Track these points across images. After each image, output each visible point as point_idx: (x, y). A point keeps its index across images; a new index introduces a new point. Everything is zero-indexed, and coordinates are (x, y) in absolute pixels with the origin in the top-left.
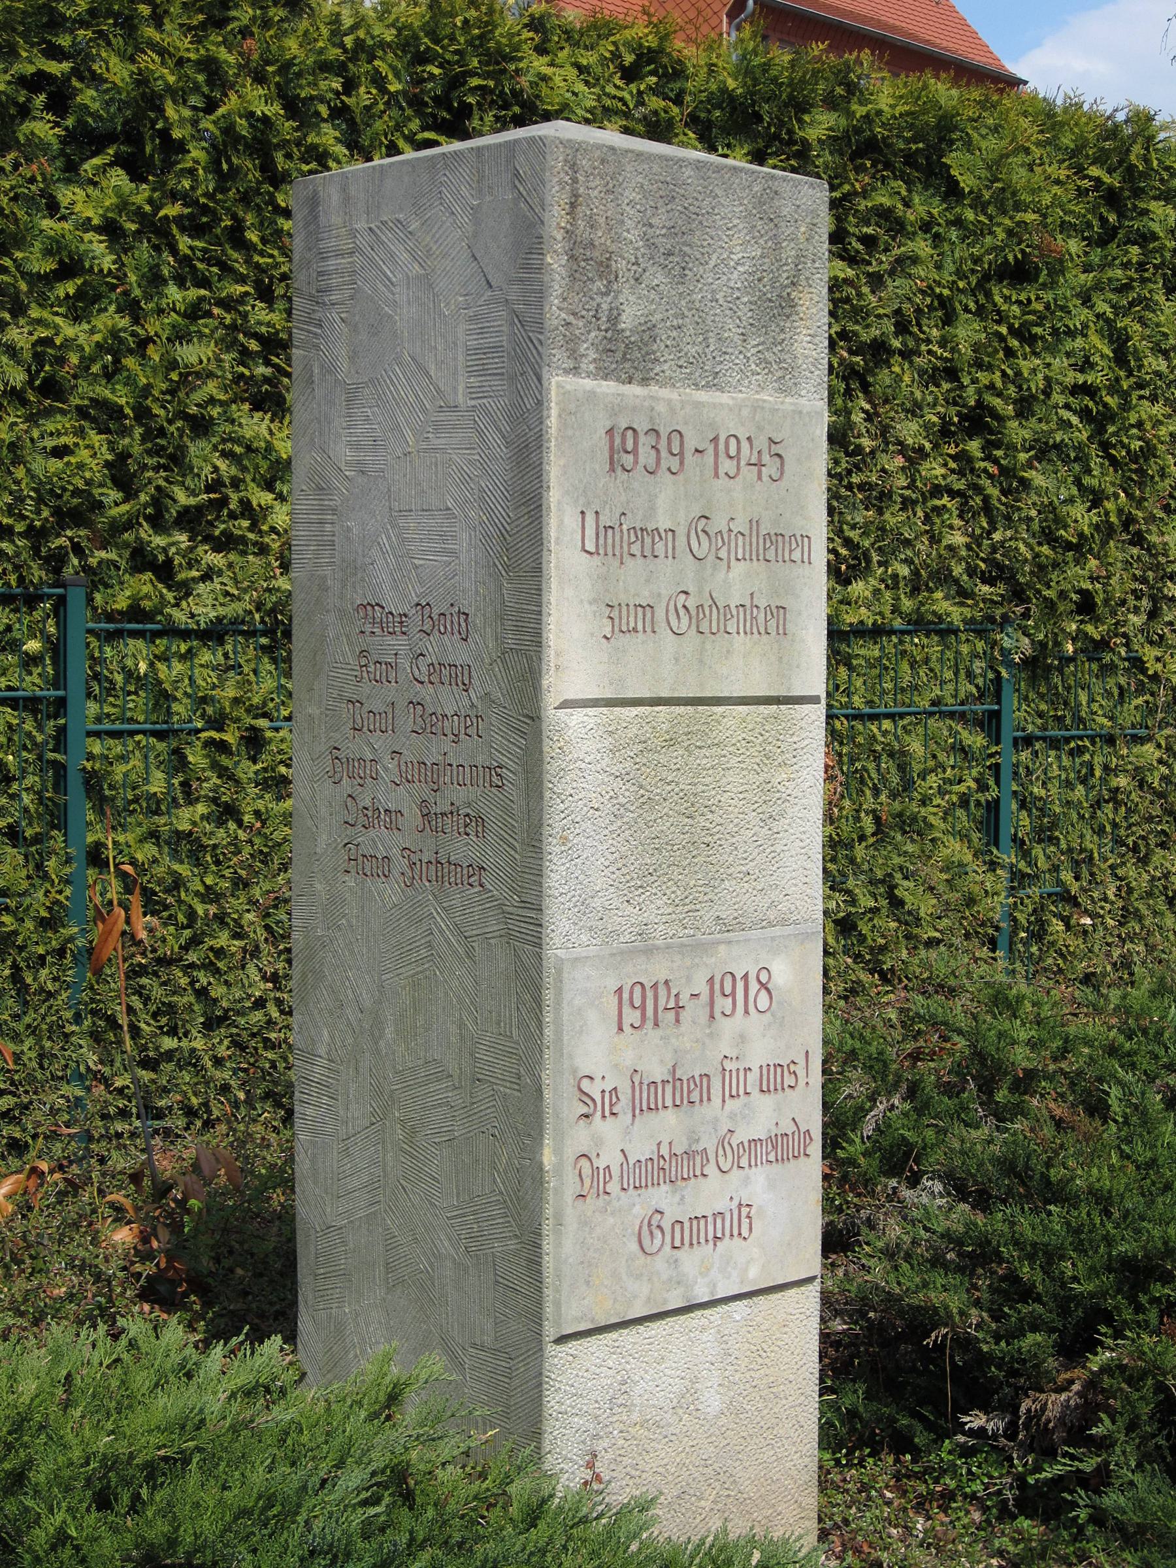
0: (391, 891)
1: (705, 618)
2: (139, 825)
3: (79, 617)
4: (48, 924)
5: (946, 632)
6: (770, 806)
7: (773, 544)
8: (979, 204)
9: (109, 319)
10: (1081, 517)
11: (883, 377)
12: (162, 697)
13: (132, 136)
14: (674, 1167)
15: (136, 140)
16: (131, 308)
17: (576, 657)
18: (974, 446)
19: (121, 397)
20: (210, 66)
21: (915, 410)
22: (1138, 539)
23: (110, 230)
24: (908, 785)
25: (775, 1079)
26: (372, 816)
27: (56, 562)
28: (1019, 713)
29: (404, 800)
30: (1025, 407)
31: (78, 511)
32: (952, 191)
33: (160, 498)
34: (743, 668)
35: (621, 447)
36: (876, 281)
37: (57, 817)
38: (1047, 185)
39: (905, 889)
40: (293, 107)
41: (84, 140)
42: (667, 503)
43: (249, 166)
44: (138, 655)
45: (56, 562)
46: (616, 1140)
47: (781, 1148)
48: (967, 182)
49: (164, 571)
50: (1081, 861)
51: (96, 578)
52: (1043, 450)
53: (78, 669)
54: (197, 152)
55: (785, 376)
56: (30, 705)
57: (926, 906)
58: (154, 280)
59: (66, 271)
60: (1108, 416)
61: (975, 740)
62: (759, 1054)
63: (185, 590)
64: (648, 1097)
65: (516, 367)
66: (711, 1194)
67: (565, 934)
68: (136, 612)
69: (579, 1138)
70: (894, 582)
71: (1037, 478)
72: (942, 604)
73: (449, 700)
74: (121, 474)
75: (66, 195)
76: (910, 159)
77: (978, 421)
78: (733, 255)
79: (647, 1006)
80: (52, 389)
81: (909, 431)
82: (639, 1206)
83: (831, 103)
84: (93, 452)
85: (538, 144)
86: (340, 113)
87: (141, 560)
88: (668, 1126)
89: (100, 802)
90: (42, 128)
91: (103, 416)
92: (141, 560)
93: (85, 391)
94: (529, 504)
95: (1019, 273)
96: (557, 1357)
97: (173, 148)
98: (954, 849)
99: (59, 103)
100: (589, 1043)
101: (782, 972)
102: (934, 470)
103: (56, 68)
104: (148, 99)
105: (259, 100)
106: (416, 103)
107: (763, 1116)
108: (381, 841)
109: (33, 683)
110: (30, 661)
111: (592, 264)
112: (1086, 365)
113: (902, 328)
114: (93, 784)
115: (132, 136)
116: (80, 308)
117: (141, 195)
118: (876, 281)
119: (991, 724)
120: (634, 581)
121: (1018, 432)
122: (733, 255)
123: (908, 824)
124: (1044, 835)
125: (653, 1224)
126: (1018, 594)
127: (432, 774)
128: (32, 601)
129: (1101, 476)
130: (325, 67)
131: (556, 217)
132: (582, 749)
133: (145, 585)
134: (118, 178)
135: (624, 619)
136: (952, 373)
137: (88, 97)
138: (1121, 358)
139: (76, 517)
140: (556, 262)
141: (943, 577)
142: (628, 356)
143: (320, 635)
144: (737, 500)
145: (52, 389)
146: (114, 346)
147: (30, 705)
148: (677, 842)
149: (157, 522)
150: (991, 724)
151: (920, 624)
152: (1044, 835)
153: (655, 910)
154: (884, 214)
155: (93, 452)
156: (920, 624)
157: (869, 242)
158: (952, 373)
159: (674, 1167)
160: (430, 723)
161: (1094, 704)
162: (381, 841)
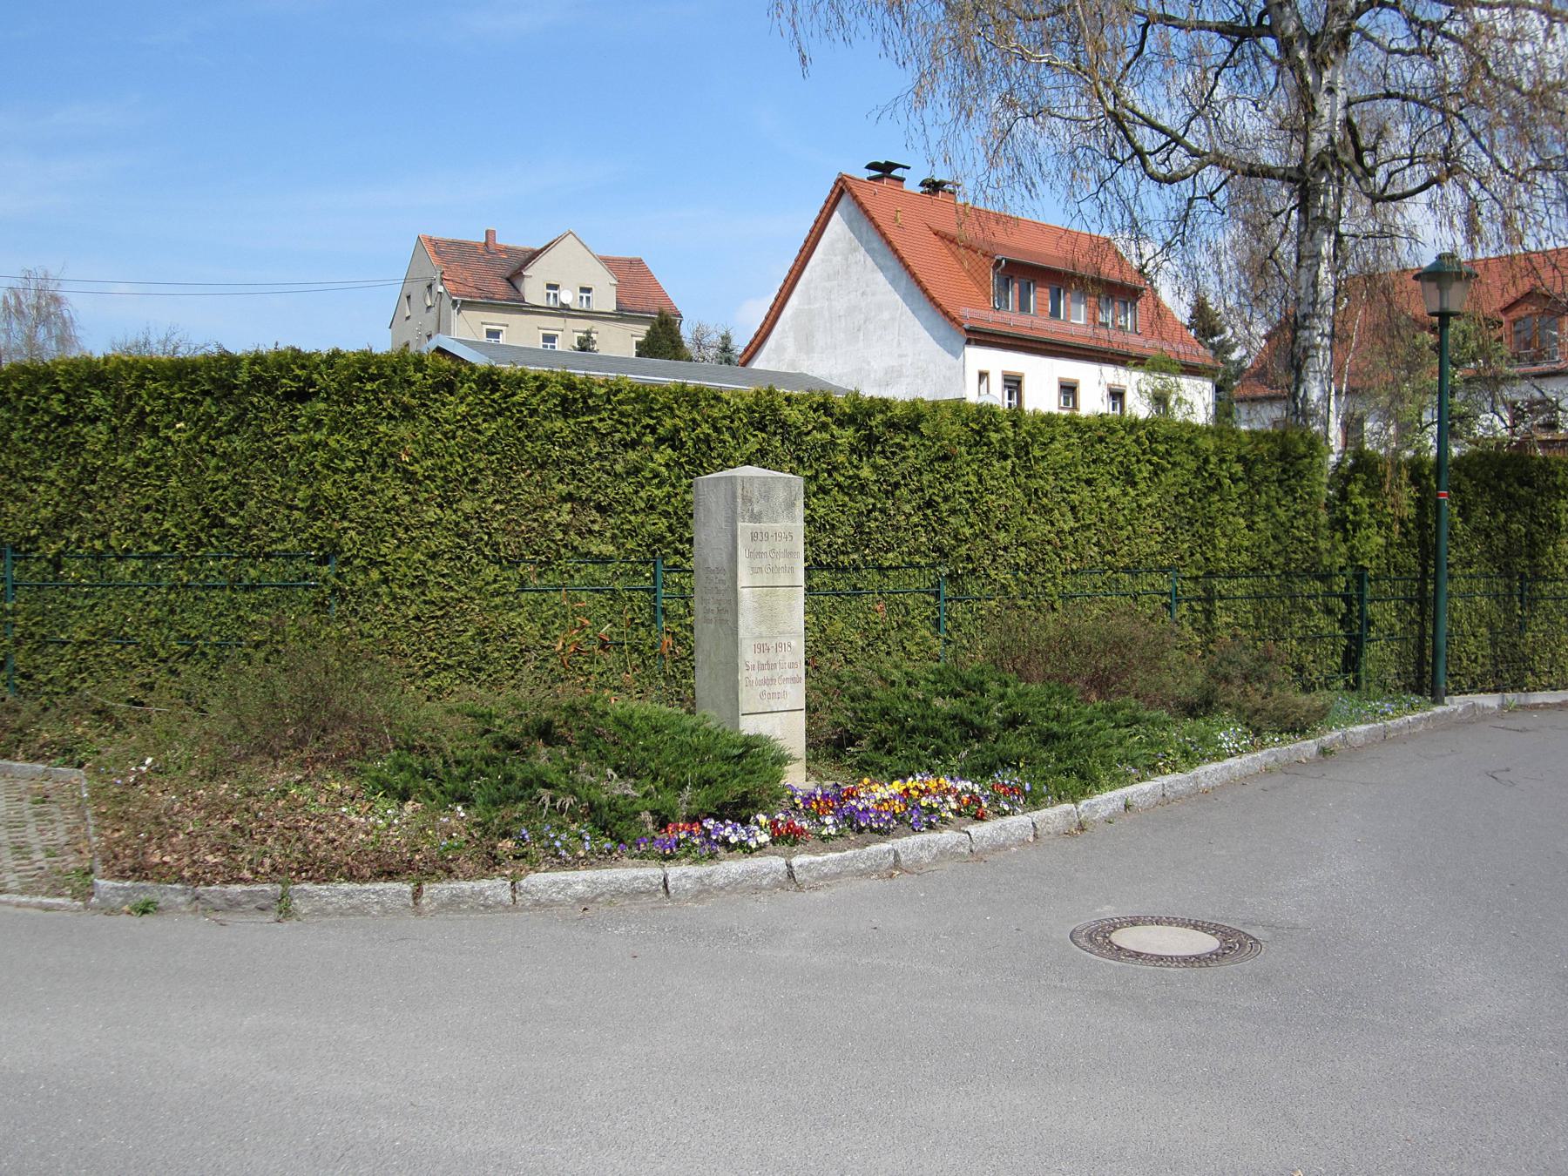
0: (712, 626)
1: (774, 570)
2: (677, 622)
3: (660, 567)
4: (652, 648)
5: (918, 566)
6: (791, 609)
7: (790, 554)
8: (929, 438)
9: (667, 488)
10: (968, 531)
11: (897, 493)
12: (683, 589)
13: (672, 439)
14: (766, 682)
15: (673, 440)
16: (673, 486)
17: (744, 578)
18: (929, 512)
19: (670, 509)
20: (693, 420)
21: (909, 502)
22: (987, 537)
23: (667, 465)
24: (908, 613)
25: (792, 665)
26: (709, 611)
27: (654, 553)
28: (946, 591)
29: (713, 607)
30: (946, 499)
31: (660, 539)
32: (922, 435)
33: (681, 536)
34: (784, 580)
35: (754, 537)
36: (896, 465)
37: (654, 620)
38: (954, 430)
39: (906, 644)
40: (716, 429)
41: (661, 441)
42: (765, 547)
43: (704, 448)
44: (676, 577)
45: (654, 553)
46: (755, 675)
47: (794, 680)
48: (925, 432)
49: (683, 555)
50: (969, 637)
51: (664, 557)
52: (953, 512)
53: (660, 580)
54: (690, 443)
55: (793, 519)
56: (647, 590)
57: (914, 649)
58: (679, 478)
59: (655, 477)
60: (974, 500)
61: (932, 600)
62: (789, 660)
63: (688, 559)
64: (761, 667)
65: (733, 521)
66: (777, 688)
67: (742, 633)
68: (675, 566)
69: (746, 674)
70: (902, 553)
71: (951, 520)
72: (917, 559)
73: (722, 587)
74: (671, 529)
75: (656, 456)
76: (907, 427)
77: (930, 504)
78: (780, 495)
79: (762, 648)
80: (652, 508)
81: (907, 508)
82: (760, 689)
83: (881, 412)
84: (663, 524)
85: (731, 479)
86: (729, 428)
87: (676, 551)
88: (766, 673)
89: (667, 617)
90: (649, 439)
91: (666, 514)
92: (676, 551)
93: (661, 508)
94: (735, 548)
95: (945, 458)
96: (742, 718)
97: (683, 444)
98: (924, 632)
99: (653, 431)
100: (748, 655)
101: (793, 643)
102: (915, 519)
103: (652, 422)
104: (677, 430)
105: (706, 428)
106: (752, 424)
107: (790, 673)
108: (711, 616)
109: (647, 584)
110: (647, 579)
111: (747, 500)
112: (968, 485)
113: (904, 478)
114: (664, 611)
115: (672, 439)
116: (659, 486)
117: (675, 455)
118: (896, 465)
119: (937, 595)
120: (757, 562)
121: (944, 507)
122: (780, 495)
123: (908, 624)
124: (958, 627)
125: (763, 693)
126: (946, 556)
127: (719, 602)
128: (647, 563)
129: (973, 518)
130: (724, 418)
131: (739, 491)
132: (746, 596)
133: (678, 558)
134: (669, 451)
135: (755, 570)
136: (922, 490)
137: (661, 430)
138: (980, 481)
139: (658, 541)
140: (739, 501)
141: (918, 551)
142: (756, 518)
143: (700, 572)
144: (781, 546)
145: (652, 508)
146: (669, 496)
147: (647, 590)
148: (768, 615)
149: (681, 542)
150: (937, 595)
151: (911, 565)
152: (958, 627)
153: (763, 628)
154: (898, 445)
155: (663, 524)
156: (911, 565)
157: (893, 453)
158: (922, 490)
159: (769, 681)
160: (719, 592)
161: (973, 587)
162: (711, 616)
